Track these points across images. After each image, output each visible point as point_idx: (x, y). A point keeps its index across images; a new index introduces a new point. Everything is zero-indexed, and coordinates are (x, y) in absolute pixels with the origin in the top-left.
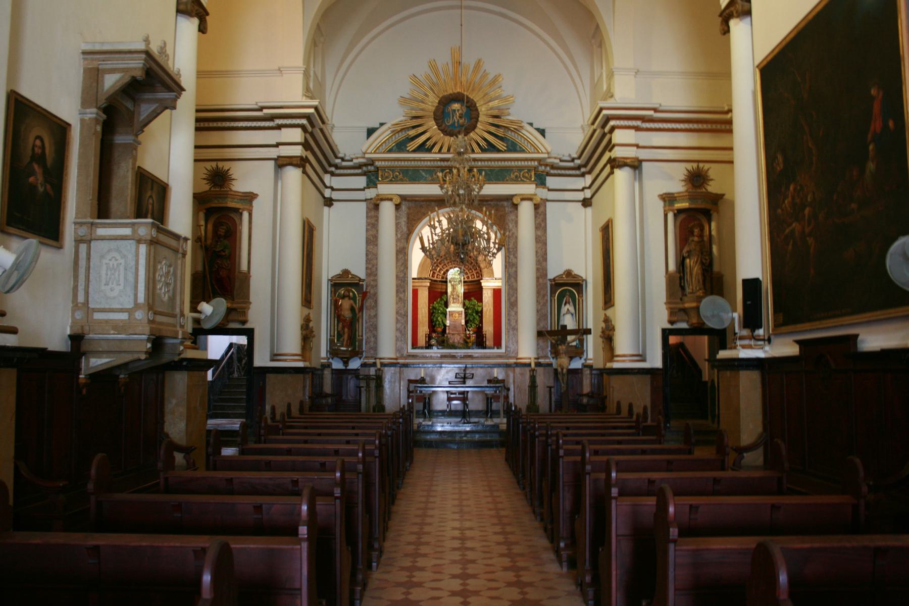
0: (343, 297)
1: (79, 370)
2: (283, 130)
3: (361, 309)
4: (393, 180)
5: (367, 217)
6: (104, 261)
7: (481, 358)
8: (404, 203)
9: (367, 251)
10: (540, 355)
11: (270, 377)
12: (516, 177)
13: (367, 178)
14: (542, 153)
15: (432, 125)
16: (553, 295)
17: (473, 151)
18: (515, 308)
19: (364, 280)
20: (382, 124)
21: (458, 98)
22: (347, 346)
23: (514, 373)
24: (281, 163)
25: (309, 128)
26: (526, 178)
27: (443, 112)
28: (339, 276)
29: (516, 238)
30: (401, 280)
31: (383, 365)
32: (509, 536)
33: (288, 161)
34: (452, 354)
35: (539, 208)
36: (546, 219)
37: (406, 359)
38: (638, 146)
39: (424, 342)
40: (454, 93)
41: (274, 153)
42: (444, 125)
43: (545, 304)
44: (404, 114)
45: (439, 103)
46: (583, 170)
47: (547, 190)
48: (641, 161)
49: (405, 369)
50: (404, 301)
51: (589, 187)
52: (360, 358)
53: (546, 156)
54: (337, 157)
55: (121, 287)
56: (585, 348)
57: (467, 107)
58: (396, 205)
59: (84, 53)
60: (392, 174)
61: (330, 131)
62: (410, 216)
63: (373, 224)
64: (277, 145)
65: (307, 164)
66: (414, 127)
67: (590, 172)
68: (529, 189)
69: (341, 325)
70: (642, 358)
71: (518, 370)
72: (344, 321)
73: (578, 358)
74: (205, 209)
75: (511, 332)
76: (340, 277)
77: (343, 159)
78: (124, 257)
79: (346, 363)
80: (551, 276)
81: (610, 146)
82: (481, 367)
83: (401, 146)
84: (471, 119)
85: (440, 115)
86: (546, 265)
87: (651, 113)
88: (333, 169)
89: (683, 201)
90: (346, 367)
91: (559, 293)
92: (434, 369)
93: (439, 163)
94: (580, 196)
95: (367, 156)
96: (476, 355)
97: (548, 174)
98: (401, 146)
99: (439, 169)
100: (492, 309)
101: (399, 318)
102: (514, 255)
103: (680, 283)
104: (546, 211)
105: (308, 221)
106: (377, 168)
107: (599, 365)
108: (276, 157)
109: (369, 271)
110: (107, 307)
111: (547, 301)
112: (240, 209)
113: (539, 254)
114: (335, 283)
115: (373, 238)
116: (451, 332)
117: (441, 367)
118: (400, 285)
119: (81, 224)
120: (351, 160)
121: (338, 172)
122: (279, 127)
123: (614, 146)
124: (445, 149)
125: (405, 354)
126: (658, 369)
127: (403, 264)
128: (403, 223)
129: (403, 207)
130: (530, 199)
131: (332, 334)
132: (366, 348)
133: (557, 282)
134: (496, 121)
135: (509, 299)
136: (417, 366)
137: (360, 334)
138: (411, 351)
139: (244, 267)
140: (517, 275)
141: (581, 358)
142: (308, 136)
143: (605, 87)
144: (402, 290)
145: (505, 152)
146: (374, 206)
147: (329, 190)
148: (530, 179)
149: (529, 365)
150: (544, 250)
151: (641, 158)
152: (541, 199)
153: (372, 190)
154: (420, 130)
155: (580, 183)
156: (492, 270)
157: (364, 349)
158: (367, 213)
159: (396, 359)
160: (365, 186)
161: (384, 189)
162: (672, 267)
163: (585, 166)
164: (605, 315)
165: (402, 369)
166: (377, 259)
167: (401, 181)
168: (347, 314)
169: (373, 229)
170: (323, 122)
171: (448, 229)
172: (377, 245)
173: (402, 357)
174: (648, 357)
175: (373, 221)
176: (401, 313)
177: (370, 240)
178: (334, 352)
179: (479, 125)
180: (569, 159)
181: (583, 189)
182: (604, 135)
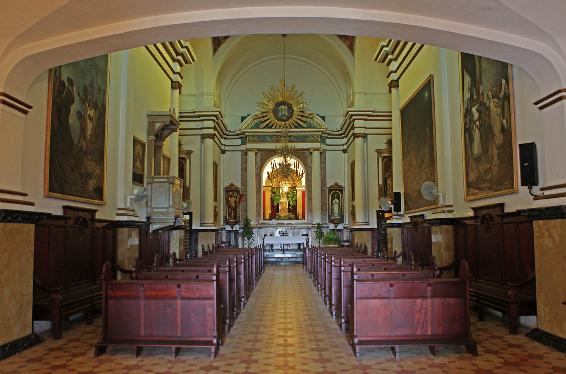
0: (231, 196)
1: (149, 229)
2: (204, 121)
3: (239, 202)
5: (242, 159)
6: (157, 190)
8: (259, 152)
9: (242, 174)
11: (200, 234)
12: (311, 139)
14: (324, 128)
15: (271, 115)
17: (291, 128)
20: (249, 115)
21: (283, 103)
22: (233, 219)
23: (311, 231)
24: (204, 137)
25: (216, 120)
26: (316, 140)
27: (277, 110)
29: (312, 168)
32: (323, 353)
33: (206, 136)
38: (365, 128)
40: (282, 101)
41: (200, 132)
42: (277, 116)
43: (325, 199)
45: (275, 105)
46: (343, 136)
48: (367, 134)
49: (260, 230)
51: (346, 144)
53: (325, 130)
54: (227, 131)
55: (164, 200)
56: (344, 220)
57: (288, 107)
58: (255, 153)
59: (148, 116)
63: (244, 162)
64: (202, 129)
65: (215, 137)
66: (263, 117)
67: (346, 137)
68: (317, 145)
69: (230, 210)
72: (232, 207)
73: (341, 224)
77: (230, 132)
78: (164, 189)
79: (232, 227)
80: (328, 186)
81: (353, 128)
83: (257, 126)
84: (290, 113)
85: (275, 112)
87: (371, 113)
88: (225, 136)
89: (386, 153)
93: (275, 134)
95: (241, 130)
96: (293, 223)
97: (327, 138)
98: (257, 126)
99: (275, 136)
100: (301, 200)
101: (257, 206)
105: (215, 161)
106: (246, 137)
108: (201, 134)
109: (243, 184)
110: (159, 207)
111: (326, 197)
113: (322, 176)
114: (227, 190)
116: (282, 212)
117: (277, 229)
119: (149, 177)
120: (234, 132)
121: (228, 137)
122: (202, 120)
123: (354, 128)
124: (278, 127)
125: (260, 223)
128: (259, 161)
129: (259, 154)
130: (318, 150)
131: (226, 214)
134: (301, 114)
135: (309, 197)
142: (215, 123)
143: (352, 99)
144: (258, 193)
145: (306, 128)
146: (245, 153)
147: (224, 146)
148: (318, 141)
151: (367, 133)
152: (323, 150)
153: (244, 146)
154: (266, 118)
156: (301, 182)
157: (241, 221)
158: (242, 157)
159: (256, 225)
160: (241, 144)
161: (249, 146)
162: (381, 183)
163: (344, 134)
164: (352, 204)
166: (246, 178)
167: (258, 142)
168: (233, 204)
169: (245, 164)
170: (222, 117)
171: (280, 169)
172: (246, 172)
173: (259, 224)
179: (294, 116)
180: (336, 130)
181: (343, 145)
182: (351, 122)
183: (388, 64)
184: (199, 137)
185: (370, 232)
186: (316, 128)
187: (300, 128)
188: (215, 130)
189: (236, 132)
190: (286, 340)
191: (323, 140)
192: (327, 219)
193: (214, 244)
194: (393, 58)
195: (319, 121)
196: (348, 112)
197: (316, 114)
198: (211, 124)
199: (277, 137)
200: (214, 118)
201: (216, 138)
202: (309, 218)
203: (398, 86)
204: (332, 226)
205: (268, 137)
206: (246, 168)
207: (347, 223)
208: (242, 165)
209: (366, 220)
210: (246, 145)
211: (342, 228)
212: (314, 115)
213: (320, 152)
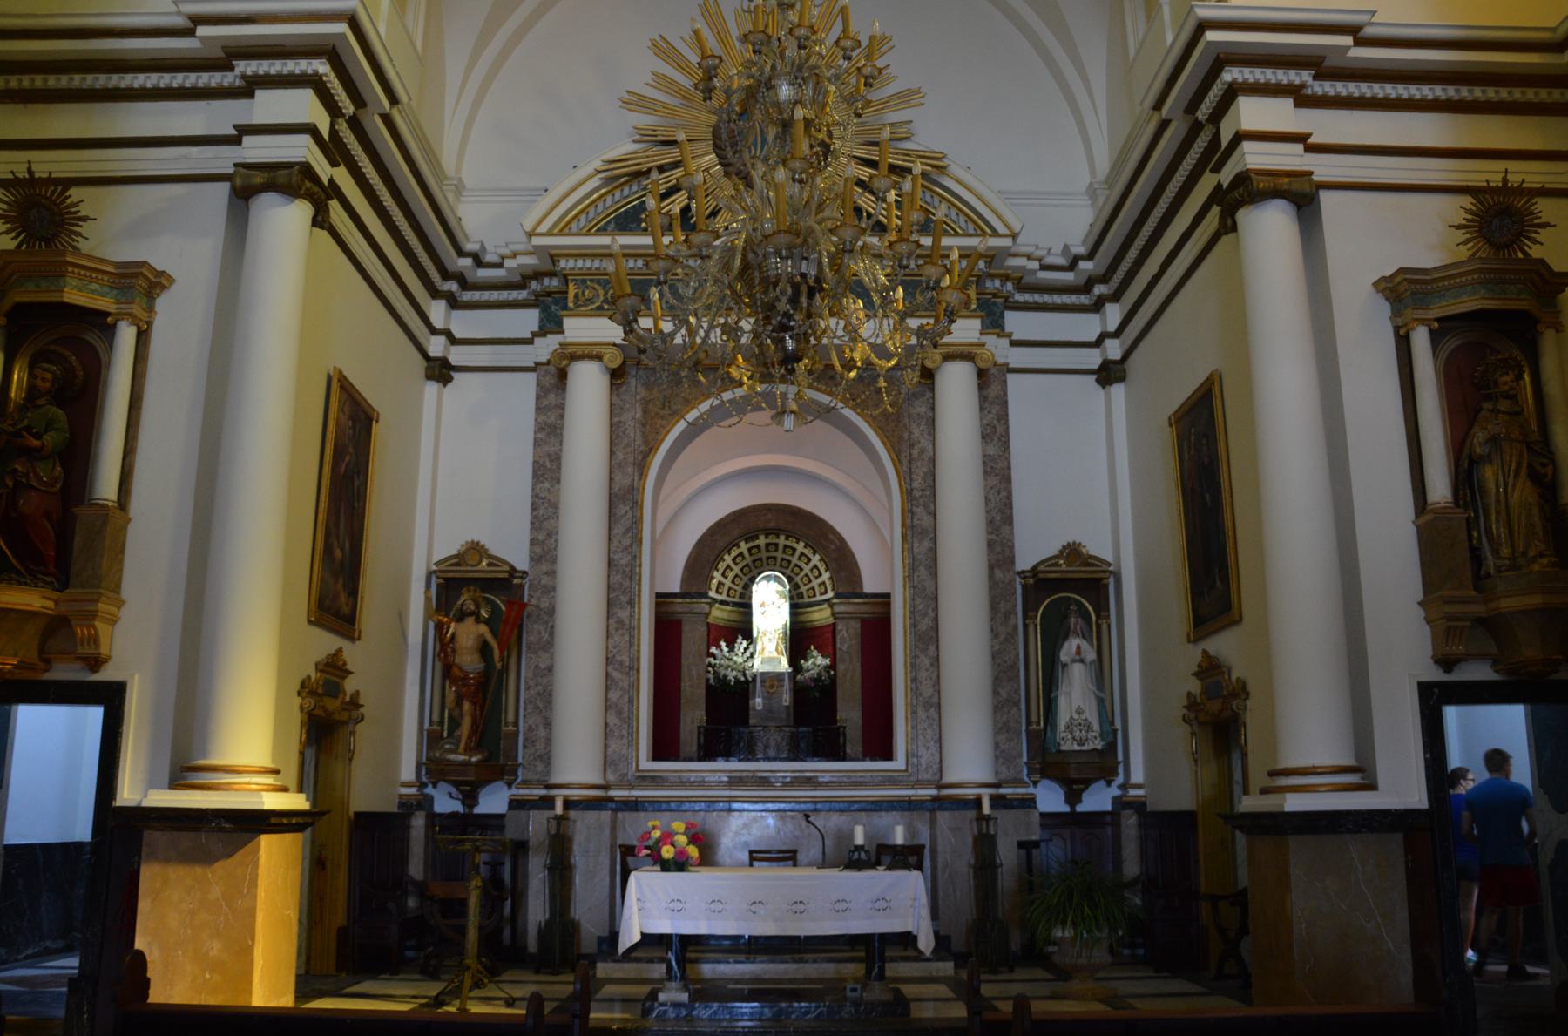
4: (606, 307)
5: (538, 409)
7: (840, 785)
9: (535, 496)
10: (1002, 777)
13: (542, 311)
14: (995, 233)
16: (1031, 614)
18: (932, 648)
19: (525, 572)
22: (468, 750)
28: (456, 560)
30: (624, 572)
31: (569, 804)
33: (259, 178)
34: (760, 774)
35: (990, 380)
36: (1007, 415)
37: (632, 789)
39: (695, 748)
41: (222, 159)
44: (637, 137)
46: (1099, 289)
47: (1006, 341)
50: (631, 628)
51: (1117, 334)
52: (510, 785)
53: (1007, 242)
54: (461, 253)
60: (601, 292)
61: (451, 197)
62: (650, 406)
65: (334, 205)
67: (1116, 297)
70: (1363, 774)
71: (944, 818)
73: (1102, 783)
74: (4, 315)
75: (921, 713)
76: (458, 564)
80: (1024, 561)
81: (1217, 155)
82: (841, 811)
86: (1012, 533)
88: (453, 286)
90: (472, 806)
91: (1052, 601)
92: (708, 814)
94: (1093, 359)
95: (536, 241)
96: (827, 778)
102: (925, 506)
103: (1470, 537)
104: (1005, 394)
107: (1180, 794)
109: (538, 550)
111: (1015, 628)
112: (108, 314)
115: (551, 461)
117: (730, 810)
118: (621, 584)
120: (500, 265)
121: (468, 296)
126: (78, 846)
127: (627, 531)
131: (436, 718)
132: (523, 758)
133: (1041, 576)
135: (914, 625)
136: (664, 806)
137: (511, 718)
138: (647, 764)
139: (106, 487)
140: (935, 560)
141: (1109, 783)
144: (624, 599)
146: (555, 377)
147: (442, 339)
149: (978, 802)
150: (1004, 494)
155: (1087, 326)
157: (520, 760)
158: (538, 398)
159: (605, 787)
160: (536, 329)
162: (1440, 488)
163: (1104, 279)
165: (620, 815)
168: (469, 661)
170: (394, 100)
172: (559, 481)
174: (1382, 779)
175: (553, 419)
176: (621, 663)
177: (545, 467)
178: (433, 770)
180: (1062, 261)
182: (1196, 128)
184: (220, 193)
192: (1020, 756)
196: (1202, 27)
204: (1050, 798)
206: (557, 459)
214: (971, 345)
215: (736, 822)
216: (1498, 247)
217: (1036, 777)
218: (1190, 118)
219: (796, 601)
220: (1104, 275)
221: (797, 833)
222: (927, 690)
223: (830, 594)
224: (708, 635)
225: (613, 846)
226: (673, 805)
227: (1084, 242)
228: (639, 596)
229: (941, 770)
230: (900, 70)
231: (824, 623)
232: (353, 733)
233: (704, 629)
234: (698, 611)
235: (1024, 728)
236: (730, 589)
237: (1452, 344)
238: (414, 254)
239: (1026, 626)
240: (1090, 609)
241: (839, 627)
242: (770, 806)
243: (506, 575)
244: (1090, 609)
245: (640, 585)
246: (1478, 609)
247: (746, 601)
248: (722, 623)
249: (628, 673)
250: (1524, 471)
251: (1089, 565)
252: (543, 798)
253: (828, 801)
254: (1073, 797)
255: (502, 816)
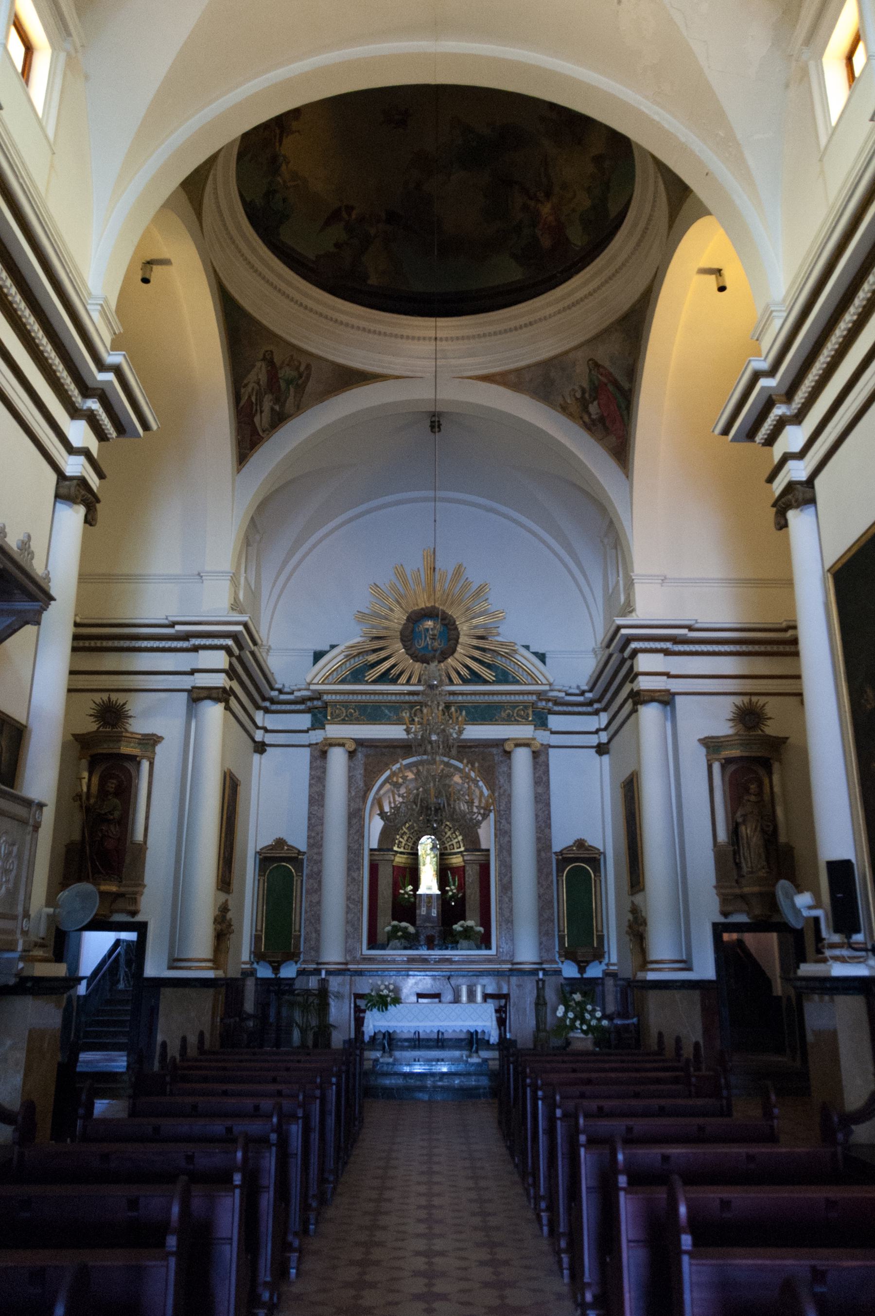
2: (201, 652)
4: (347, 719)
5: (311, 768)
8: (360, 749)
9: (310, 813)
10: (544, 959)
14: (542, 684)
20: (333, 647)
21: (429, 613)
25: (236, 651)
27: (413, 631)
31: (329, 973)
33: (204, 694)
35: (540, 757)
38: (668, 675)
40: (427, 608)
41: (187, 682)
42: (413, 649)
43: (549, 886)
44: (362, 634)
46: (596, 706)
47: (549, 732)
49: (357, 978)
51: (606, 729)
52: (296, 962)
53: (547, 688)
54: (272, 689)
56: (606, 949)
57: (442, 624)
60: (344, 711)
61: (264, 654)
64: (192, 672)
65: (232, 698)
66: (375, 651)
67: (605, 710)
68: (524, 731)
70: (686, 965)
73: (597, 962)
76: (271, 850)
77: (281, 692)
82: (464, 976)
83: (357, 676)
87: (684, 631)
88: (267, 704)
90: (276, 974)
91: (567, 874)
93: (407, 698)
94: (594, 740)
95: (312, 687)
96: (457, 958)
98: (357, 676)
99: (407, 705)
101: (351, 906)
102: (506, 819)
104: (548, 760)
105: (231, 773)
106: (326, 704)
108: (189, 687)
109: (312, 841)
111: (552, 882)
112: (137, 756)
117: (408, 975)
120: (292, 693)
121: (274, 707)
122: (196, 649)
124: (414, 680)
125: (358, 956)
128: (359, 776)
130: (527, 745)
131: (259, 928)
135: (500, 880)
137: (297, 928)
138: (366, 952)
139: (139, 836)
141: (601, 962)
143: (622, 599)
146: (321, 753)
147: (262, 732)
150: (547, 812)
151: (673, 691)
152: (542, 745)
154: (383, 654)
157: (302, 949)
159: (346, 964)
161: (334, 731)
162: (722, 836)
163: (599, 701)
165: (353, 978)
167: (357, 721)
170: (255, 643)
172: (323, 806)
178: (258, 956)
179: (459, 649)
180: (577, 692)
182: (623, 661)
183: (770, 441)
185: (698, 992)
186: (521, 684)
187: (476, 683)
188: (231, 679)
189: (297, 694)
190: (430, 1264)
191: (542, 718)
192: (554, 948)
193: (207, 1035)
194: (788, 413)
195: (529, 666)
196: (619, 628)
197: (523, 646)
198: (220, 660)
199: (411, 708)
200: (230, 642)
201: (233, 702)
202: (504, 945)
203: (812, 501)
205: (387, 707)
207: (614, 959)
208: (311, 785)
209: (682, 956)
210: (324, 729)
211: (600, 975)
212: (516, 647)
213: (534, 752)
214: (529, 739)
215: (411, 981)
216: (749, 728)
217: (563, 959)
218: (620, 656)
219: (443, 851)
220: (599, 698)
221: (442, 987)
222: (507, 914)
223: (462, 849)
224: (393, 873)
225: (350, 993)
226: (379, 973)
227: (587, 684)
228: (363, 866)
229: (513, 955)
230: (495, 600)
231: (458, 865)
232: (229, 939)
233: (391, 870)
234: (387, 858)
235: (556, 933)
236: (405, 844)
237: (732, 768)
238: (252, 695)
239: (558, 881)
240: (591, 871)
241: (467, 868)
242: (428, 973)
243: (296, 855)
244: (591, 871)
245: (363, 860)
246: (737, 891)
247: (415, 851)
248: (402, 865)
249: (357, 905)
250: (759, 829)
251: (589, 850)
252: (315, 969)
253: (457, 970)
254: (582, 970)
255: (293, 979)
